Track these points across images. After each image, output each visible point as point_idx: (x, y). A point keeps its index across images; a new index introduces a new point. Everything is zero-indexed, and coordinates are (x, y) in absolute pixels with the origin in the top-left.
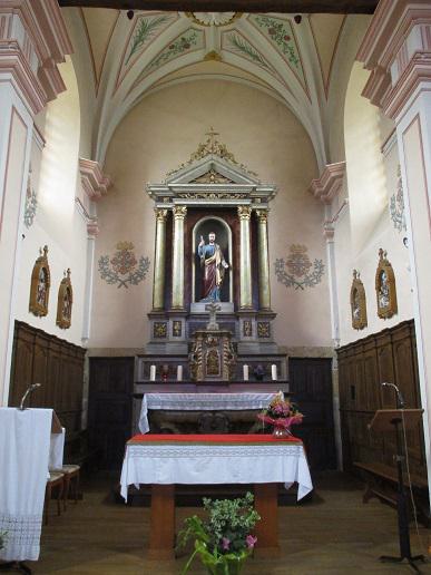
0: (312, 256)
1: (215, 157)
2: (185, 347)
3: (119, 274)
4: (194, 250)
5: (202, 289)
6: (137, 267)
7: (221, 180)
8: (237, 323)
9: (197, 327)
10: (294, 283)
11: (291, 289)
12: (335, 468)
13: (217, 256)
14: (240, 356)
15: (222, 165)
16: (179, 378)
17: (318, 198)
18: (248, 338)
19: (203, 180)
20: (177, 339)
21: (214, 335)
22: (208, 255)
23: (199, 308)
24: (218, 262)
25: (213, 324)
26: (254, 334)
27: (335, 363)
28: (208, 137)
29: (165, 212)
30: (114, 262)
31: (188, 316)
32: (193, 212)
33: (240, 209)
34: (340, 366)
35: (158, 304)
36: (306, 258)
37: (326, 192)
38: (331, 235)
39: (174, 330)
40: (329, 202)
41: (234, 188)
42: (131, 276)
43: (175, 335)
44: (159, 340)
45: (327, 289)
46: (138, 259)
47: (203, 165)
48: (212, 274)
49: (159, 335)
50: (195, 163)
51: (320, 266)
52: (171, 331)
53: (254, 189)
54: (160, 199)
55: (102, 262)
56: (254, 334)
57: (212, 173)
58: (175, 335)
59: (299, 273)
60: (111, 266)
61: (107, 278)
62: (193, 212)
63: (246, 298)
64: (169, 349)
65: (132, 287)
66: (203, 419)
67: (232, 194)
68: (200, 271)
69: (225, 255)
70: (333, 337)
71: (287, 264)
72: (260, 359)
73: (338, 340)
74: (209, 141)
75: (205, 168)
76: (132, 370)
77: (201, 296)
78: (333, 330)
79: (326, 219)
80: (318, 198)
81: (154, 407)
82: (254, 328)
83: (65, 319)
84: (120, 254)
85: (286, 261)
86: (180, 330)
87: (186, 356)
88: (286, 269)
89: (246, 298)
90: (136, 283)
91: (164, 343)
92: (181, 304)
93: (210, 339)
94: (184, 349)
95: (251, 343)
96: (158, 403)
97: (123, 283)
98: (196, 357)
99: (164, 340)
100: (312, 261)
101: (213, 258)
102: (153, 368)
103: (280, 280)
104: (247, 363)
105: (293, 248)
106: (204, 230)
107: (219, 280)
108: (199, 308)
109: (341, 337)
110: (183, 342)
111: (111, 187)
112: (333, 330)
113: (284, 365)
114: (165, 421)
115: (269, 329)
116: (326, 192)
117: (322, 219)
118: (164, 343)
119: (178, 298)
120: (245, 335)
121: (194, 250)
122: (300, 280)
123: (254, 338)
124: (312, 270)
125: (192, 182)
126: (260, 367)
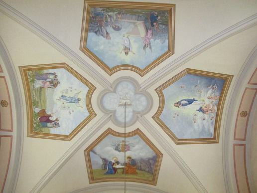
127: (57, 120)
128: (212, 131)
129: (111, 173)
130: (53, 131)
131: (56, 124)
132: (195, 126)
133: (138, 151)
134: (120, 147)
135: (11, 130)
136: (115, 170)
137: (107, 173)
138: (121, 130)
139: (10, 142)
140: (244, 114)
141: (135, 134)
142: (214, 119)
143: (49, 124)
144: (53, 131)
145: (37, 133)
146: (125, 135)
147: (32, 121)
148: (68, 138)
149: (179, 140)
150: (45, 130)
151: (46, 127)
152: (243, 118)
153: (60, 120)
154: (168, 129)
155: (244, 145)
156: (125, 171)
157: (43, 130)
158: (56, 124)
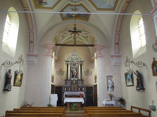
0: (90, 71)
5: (73, 76)
6: (63, 72)
9: (72, 82)
11: (87, 76)
13: (75, 71)
16: (69, 90)
23: (72, 79)
30: (59, 71)
48: (74, 74)
49: (66, 83)
51: (91, 72)
63: (79, 78)
64: (68, 86)
68: (73, 73)
76: (62, 89)
80: (91, 61)
88: (86, 73)
94: (70, 86)
105: (87, 69)
108: (72, 79)
111: (58, 59)
119: (69, 78)
127: (46, 2)
128: (113, 6)
129: (71, 17)
130: (45, 6)
131: (46, 3)
132: (106, 4)
133: (82, 12)
134: (74, 10)
135: (28, 7)
136: (72, 16)
137: (69, 17)
138: (74, 4)
139: (123, 8)
140: (117, 44)
141: (80, 5)
142: (115, 2)
143: (43, 4)
144: (45, 6)
145: (39, 7)
146: (75, 6)
147: (35, 3)
148: (52, 8)
149: (53, 7)
150: (42, 6)
151: (42, 5)
152: (117, 45)
153: (47, 2)
154: (95, 5)
155: (29, 30)
156: (75, 17)
157: (41, 6)
158: (46, 3)
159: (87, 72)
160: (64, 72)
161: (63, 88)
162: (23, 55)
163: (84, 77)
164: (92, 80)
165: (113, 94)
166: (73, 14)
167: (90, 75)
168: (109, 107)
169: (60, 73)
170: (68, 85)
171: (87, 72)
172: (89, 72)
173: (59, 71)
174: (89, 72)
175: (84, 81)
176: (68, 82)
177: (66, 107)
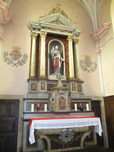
0: (93, 60)
1: (59, 14)
2: (47, 95)
3: (13, 60)
4: (49, 53)
5: (52, 69)
6: (22, 58)
7: (61, 24)
8: (38, 84)
9: (51, 87)
10: (87, 70)
11: (86, 72)
12: (103, 146)
13: (59, 56)
14: (72, 99)
15: (62, 18)
16: (46, 110)
17: (94, 39)
18: (74, 92)
19: (53, 23)
20: (43, 91)
21: (62, 90)
22: (55, 55)
23: (52, 77)
24: (60, 58)
25: (60, 85)
26: (77, 90)
27: (102, 104)
28: (57, 6)
29: (37, 35)
30: (11, 54)
31: (48, 80)
32: (49, 36)
33: (69, 37)
34: (105, 104)
35: (33, 74)
36: (91, 61)
37: (98, 36)
38: (100, 53)
39: (42, 87)
40: (98, 40)
41: (67, 28)
42: (19, 62)
43: (42, 89)
44: (33, 91)
45: (99, 74)
46: (22, 54)
47: (54, 16)
48: (57, 63)
49: (33, 89)
50: (52, 15)
51: (96, 64)
52: (40, 87)
53: (75, 29)
54: (34, 29)
55: (5, 54)
56: (77, 90)
57: (57, 21)
58: (42, 89)
59: (89, 66)
60: (9, 56)
61: (7, 62)
62: (49, 36)
63: (72, 75)
64: (40, 96)
65: (19, 66)
66: (62, 133)
67: (66, 31)
68: (52, 62)
69: (62, 56)
70: (102, 92)
71: (84, 62)
72: (80, 101)
73: (104, 93)
74: (57, 7)
75: (55, 19)
76: (18, 106)
77: (52, 72)
78: (102, 89)
79: (97, 46)
80: (94, 39)
81: (36, 128)
82: (76, 86)
83: (68, 32)
84: (14, 51)
85: (84, 61)
86: (44, 87)
87: (48, 99)
88: (84, 64)
89: (72, 75)
90: (21, 65)
91: (37, 93)
92: (44, 75)
93: (61, 91)
94: (46, 96)
95: (76, 95)
96: (40, 125)
97: (15, 64)
98: (53, 100)
99: (36, 91)
100: (93, 62)
101: (58, 56)
102: (33, 105)
103: (82, 68)
104: (76, 103)
105: (86, 56)
106: (54, 44)
107: (60, 66)
108: (52, 77)
109: (105, 92)
110: (46, 93)
111: (11, 21)
112: (102, 89)
113: (90, 103)
114: (42, 134)
115: (81, 88)
116: (98, 36)
117: (95, 47)
118: (37, 93)
119: (42, 72)
120: (73, 90)
121: (49, 53)
122: (89, 69)
123: (76, 92)
124: (93, 65)
125: (51, 23)
126: (81, 104)
159: (85, 62)
160: (27, 57)
161: (23, 106)
162: (83, 95)
163: (81, 75)
164: (100, 83)
165: (89, 95)
166: (63, 129)
167: (93, 71)
168: (109, 123)
169: (15, 59)
170: (42, 94)
171: (85, 62)
172: (92, 63)
173: (11, 54)
174: (92, 63)
175: (83, 85)
176: (71, 84)
177: (42, 133)
